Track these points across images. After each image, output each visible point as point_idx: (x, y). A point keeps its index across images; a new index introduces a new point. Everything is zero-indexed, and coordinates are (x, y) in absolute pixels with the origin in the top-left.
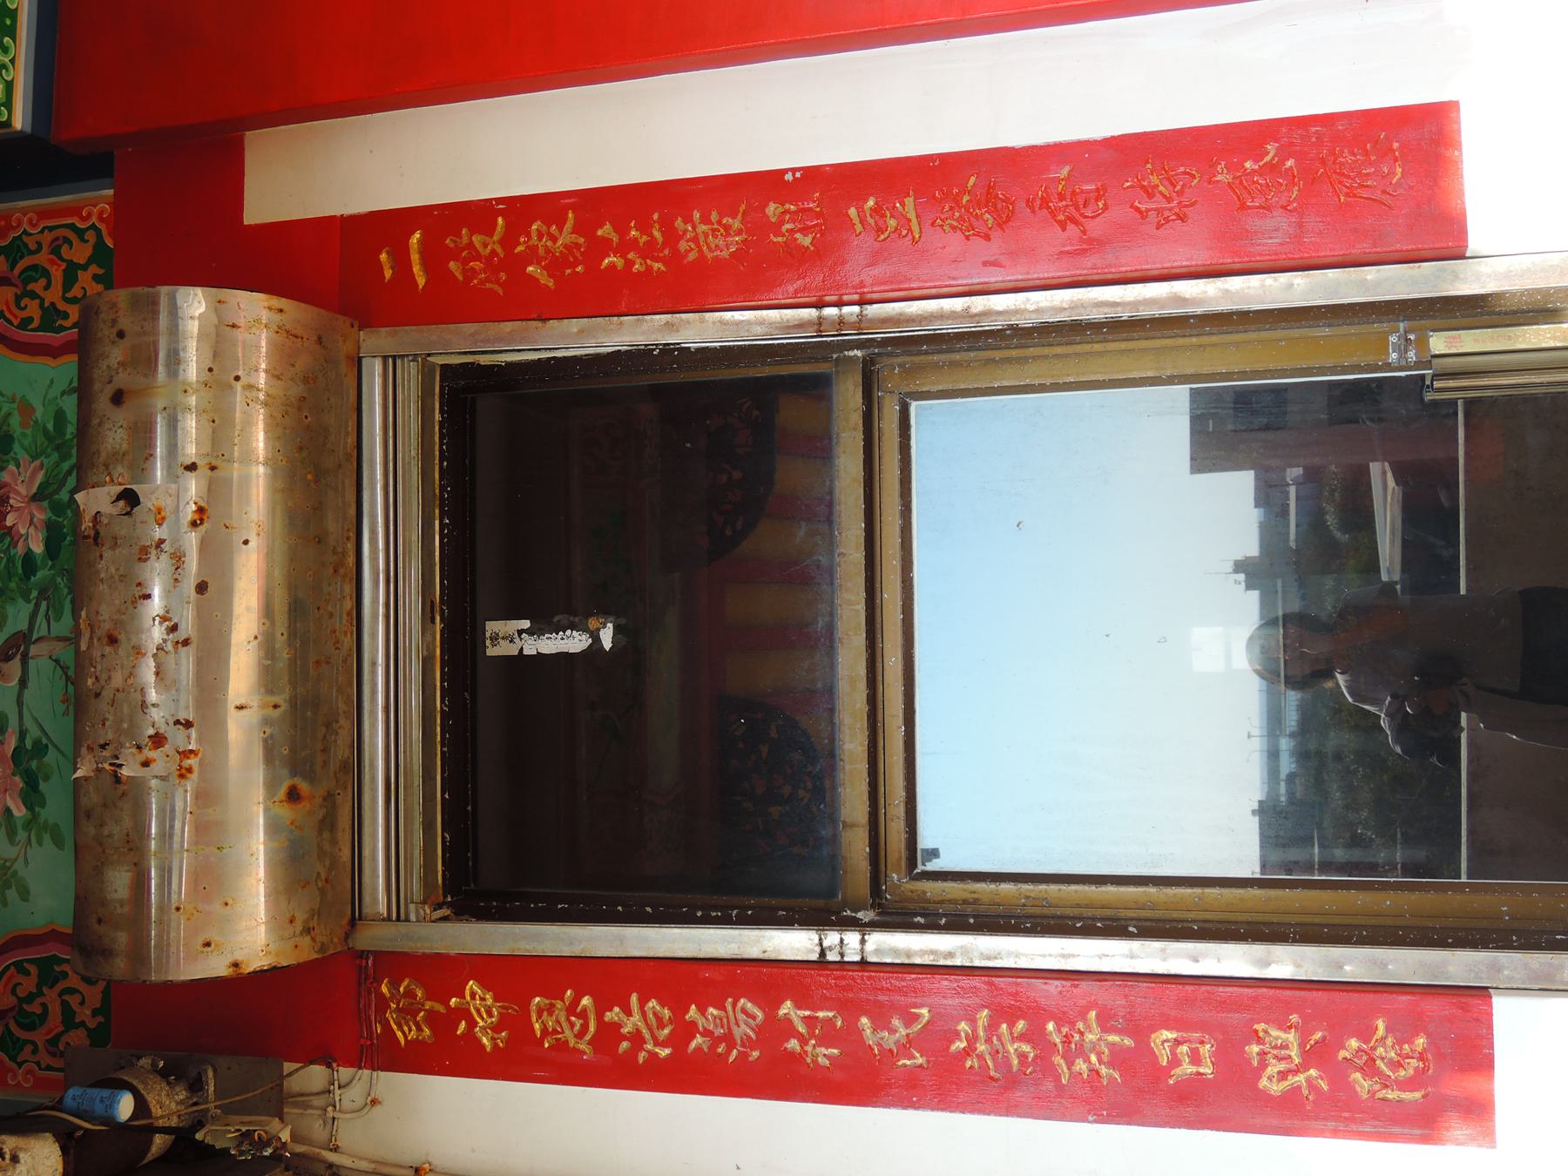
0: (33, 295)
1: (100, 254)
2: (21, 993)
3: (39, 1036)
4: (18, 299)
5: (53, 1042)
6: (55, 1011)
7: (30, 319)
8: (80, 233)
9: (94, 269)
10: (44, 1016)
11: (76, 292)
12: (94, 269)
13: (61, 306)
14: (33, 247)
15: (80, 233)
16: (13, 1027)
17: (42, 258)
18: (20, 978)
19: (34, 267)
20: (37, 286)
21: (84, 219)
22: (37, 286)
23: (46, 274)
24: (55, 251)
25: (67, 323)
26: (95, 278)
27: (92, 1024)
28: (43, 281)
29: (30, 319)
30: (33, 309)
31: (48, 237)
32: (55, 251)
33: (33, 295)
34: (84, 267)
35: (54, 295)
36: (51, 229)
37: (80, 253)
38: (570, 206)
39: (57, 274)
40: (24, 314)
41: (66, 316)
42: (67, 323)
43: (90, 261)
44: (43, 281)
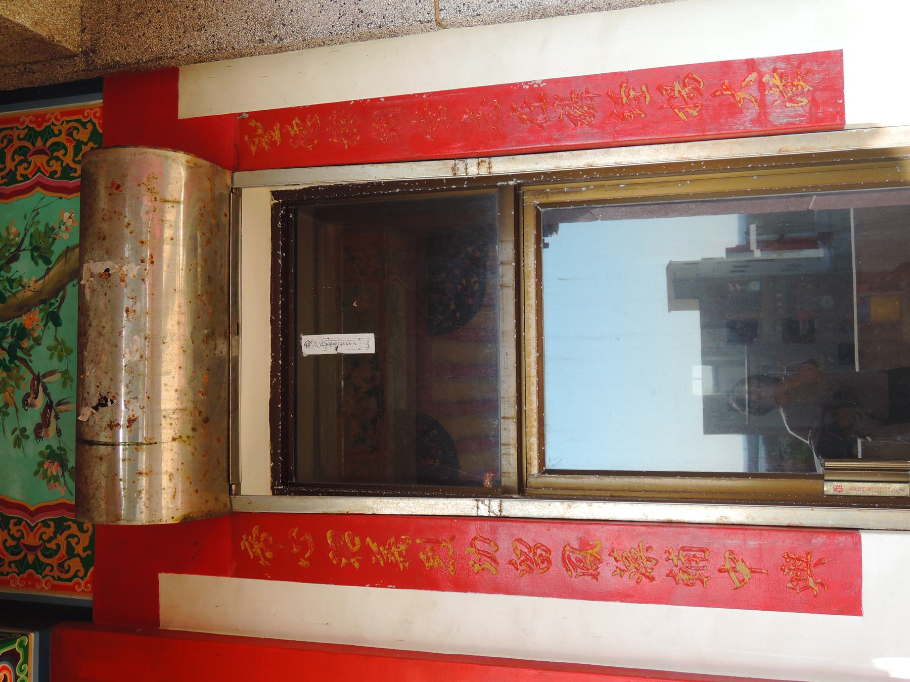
0: (57, 159)
2: (45, 537)
3: (17, 144)
7: (56, 172)
10: (15, 152)
13: (72, 165)
14: (56, 132)
16: (31, 147)
17: (62, 138)
18: (25, 172)
19: (56, 144)
22: (60, 154)
28: (62, 152)
30: (56, 166)
33: (57, 159)
34: (86, 144)
35: (68, 160)
36: (68, 122)
37: (83, 135)
39: (71, 150)
44: (7, 544)
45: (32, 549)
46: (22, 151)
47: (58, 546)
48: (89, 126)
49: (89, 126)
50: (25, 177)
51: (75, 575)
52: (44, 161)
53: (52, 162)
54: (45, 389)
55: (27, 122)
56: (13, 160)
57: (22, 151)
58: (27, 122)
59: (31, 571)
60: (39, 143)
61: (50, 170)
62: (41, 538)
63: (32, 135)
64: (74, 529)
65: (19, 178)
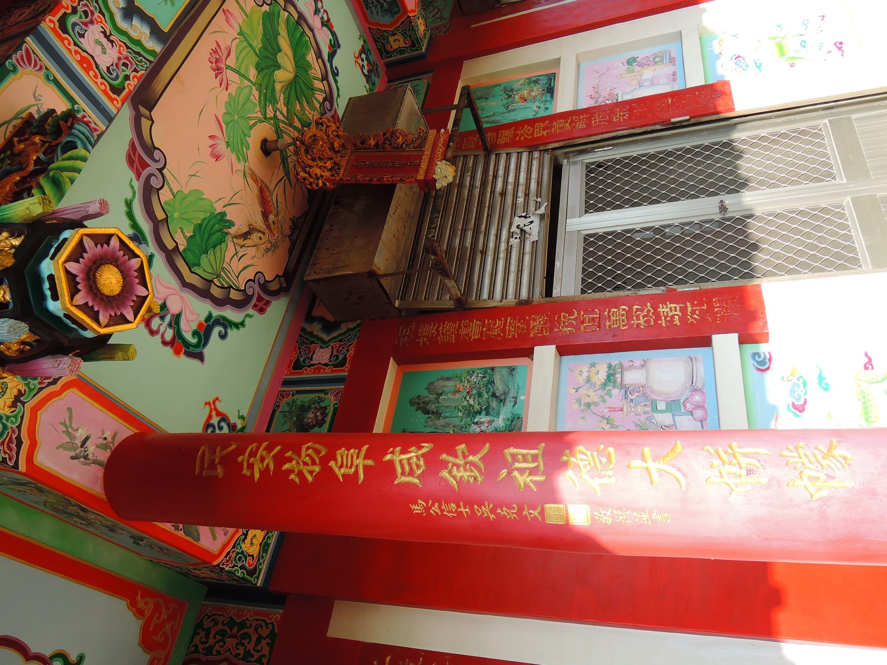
0: (243, 645)
1: (272, 636)
2: (221, 644)
3: (220, 627)
4: (237, 645)
5: (216, 624)
6: (211, 636)
7: (239, 655)
8: (267, 624)
9: (268, 640)
10: (217, 633)
11: (259, 648)
12: (268, 640)
13: (252, 652)
14: (248, 625)
15: (267, 624)
16: (229, 632)
17: (250, 631)
18: (220, 649)
19: (247, 634)
20: (245, 642)
21: (270, 619)
22: (245, 642)
23: (250, 637)
24: (256, 629)
25: (252, 660)
26: (268, 644)
27: (200, 630)
28: (248, 640)
29: (239, 655)
30: (241, 651)
31: (255, 623)
32: (256, 629)
33: (243, 645)
34: (265, 638)
35: (250, 647)
36: (257, 620)
37: (265, 632)
38: (422, 656)
39: (254, 639)
40: (238, 652)
41: (252, 656)
42: (252, 660)
43: (267, 637)
44: (248, 640)
45: (233, 636)
46: (222, 633)
47: (215, 638)
48: (270, 626)
49: (270, 626)
50: (218, 653)
51: (210, 617)
52: (235, 644)
53: (240, 646)
54: (256, 54)
55: (231, 614)
56: (215, 638)
57: (222, 633)
58: (231, 614)
59: (237, 621)
60: (235, 630)
61: (236, 651)
62: (225, 643)
63: (231, 623)
64: (201, 647)
65: (214, 652)
